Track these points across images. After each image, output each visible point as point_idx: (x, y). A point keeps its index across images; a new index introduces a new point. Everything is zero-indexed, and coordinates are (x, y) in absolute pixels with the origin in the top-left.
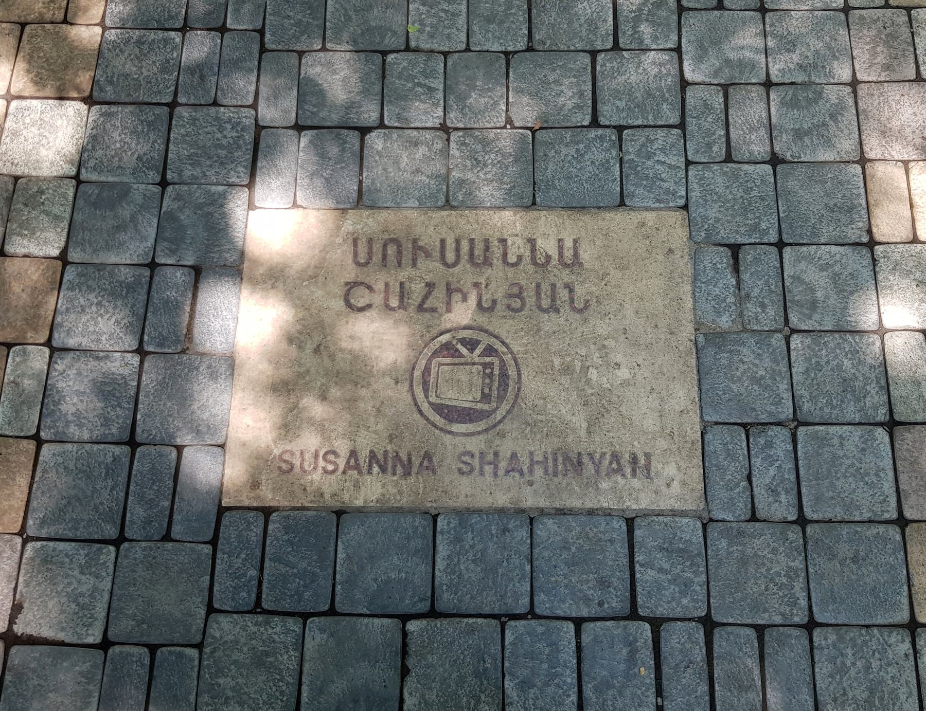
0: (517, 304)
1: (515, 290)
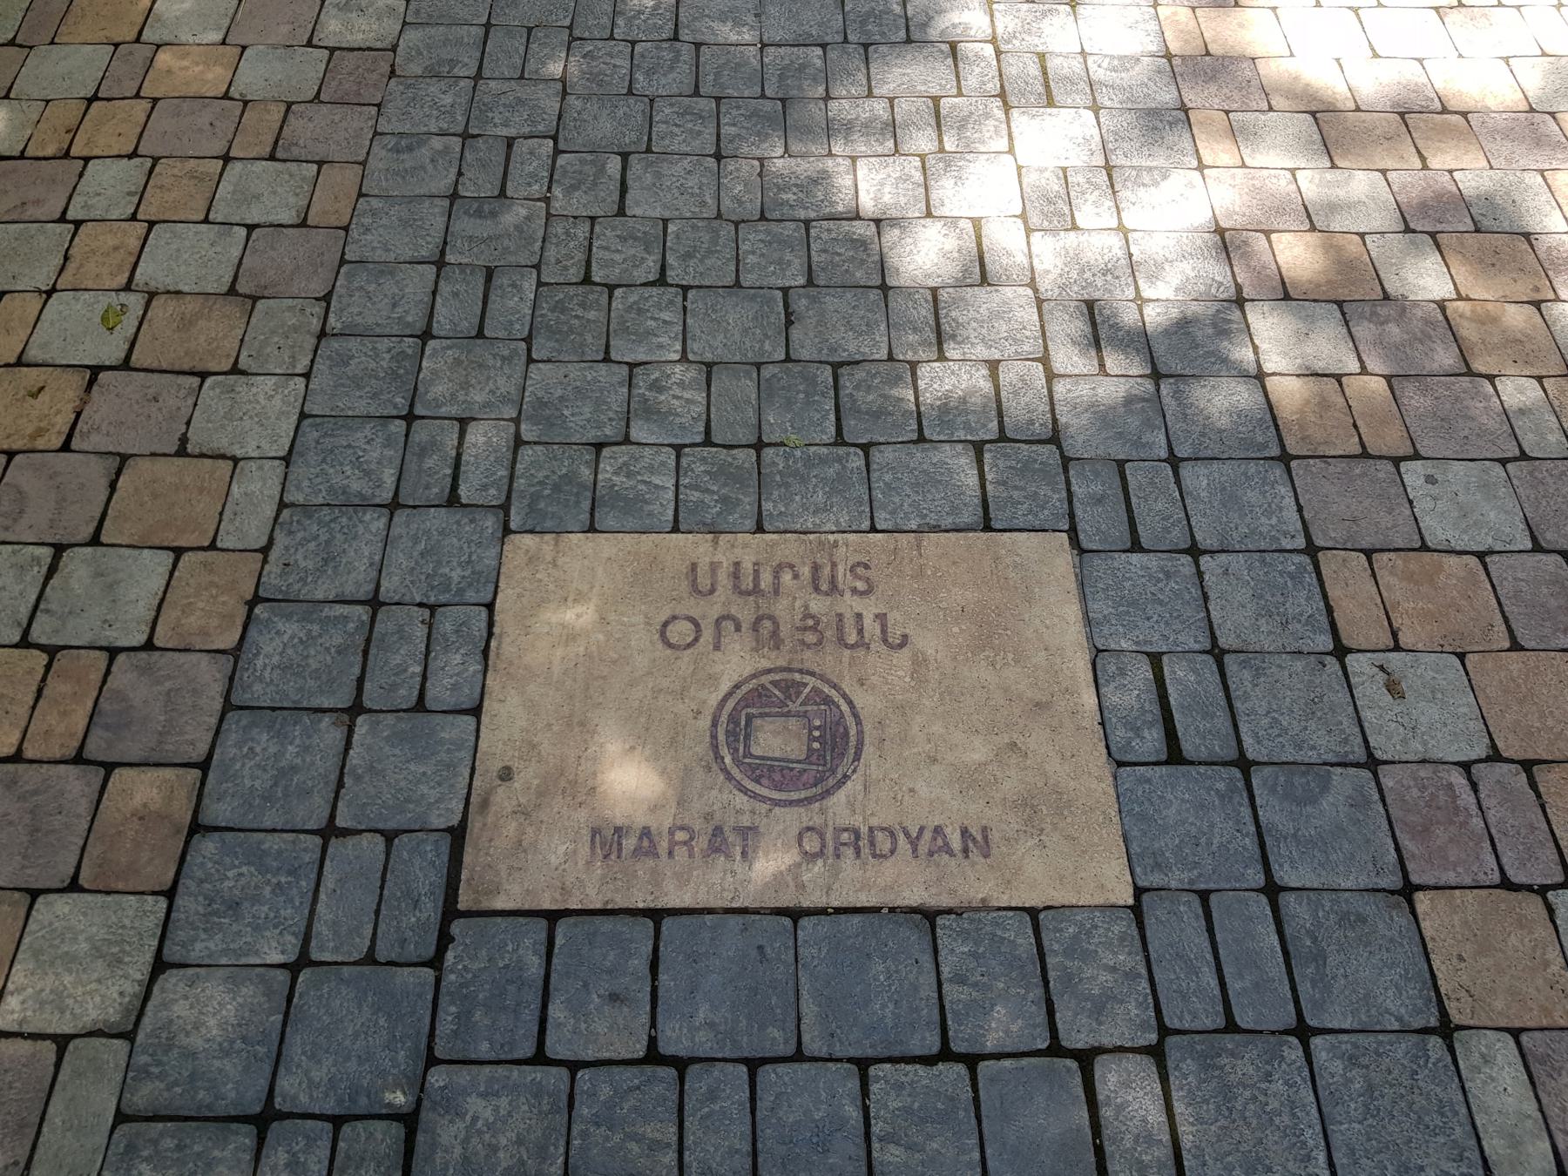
0: (811, 638)
1: (810, 622)
